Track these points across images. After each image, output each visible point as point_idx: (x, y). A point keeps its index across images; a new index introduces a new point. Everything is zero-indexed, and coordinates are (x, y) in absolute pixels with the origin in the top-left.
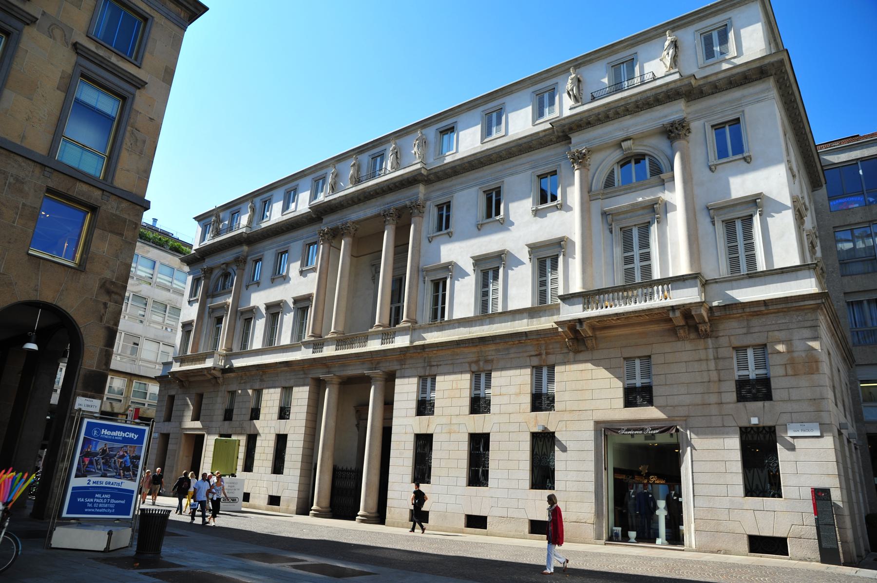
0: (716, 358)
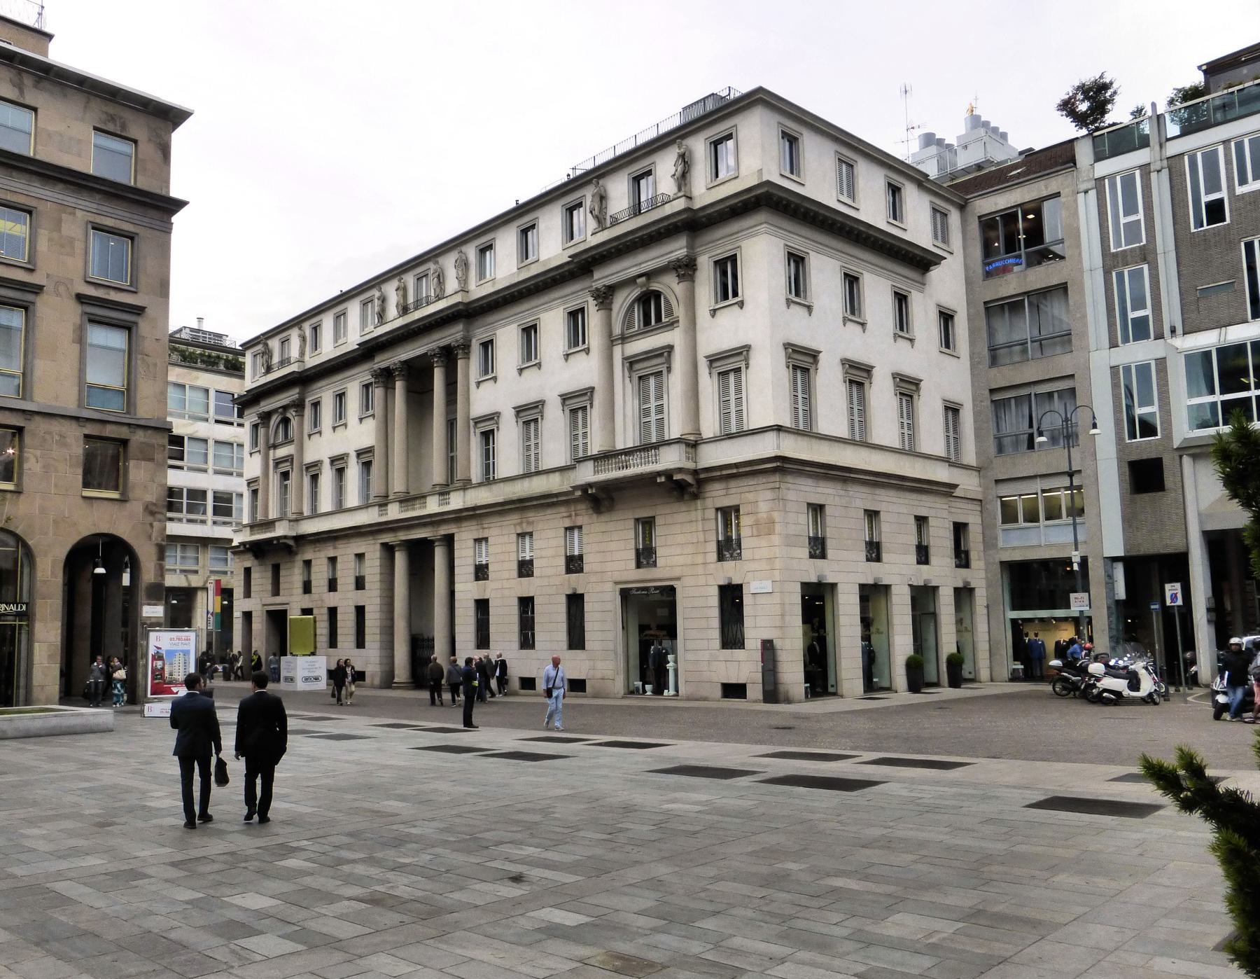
0: (703, 519)
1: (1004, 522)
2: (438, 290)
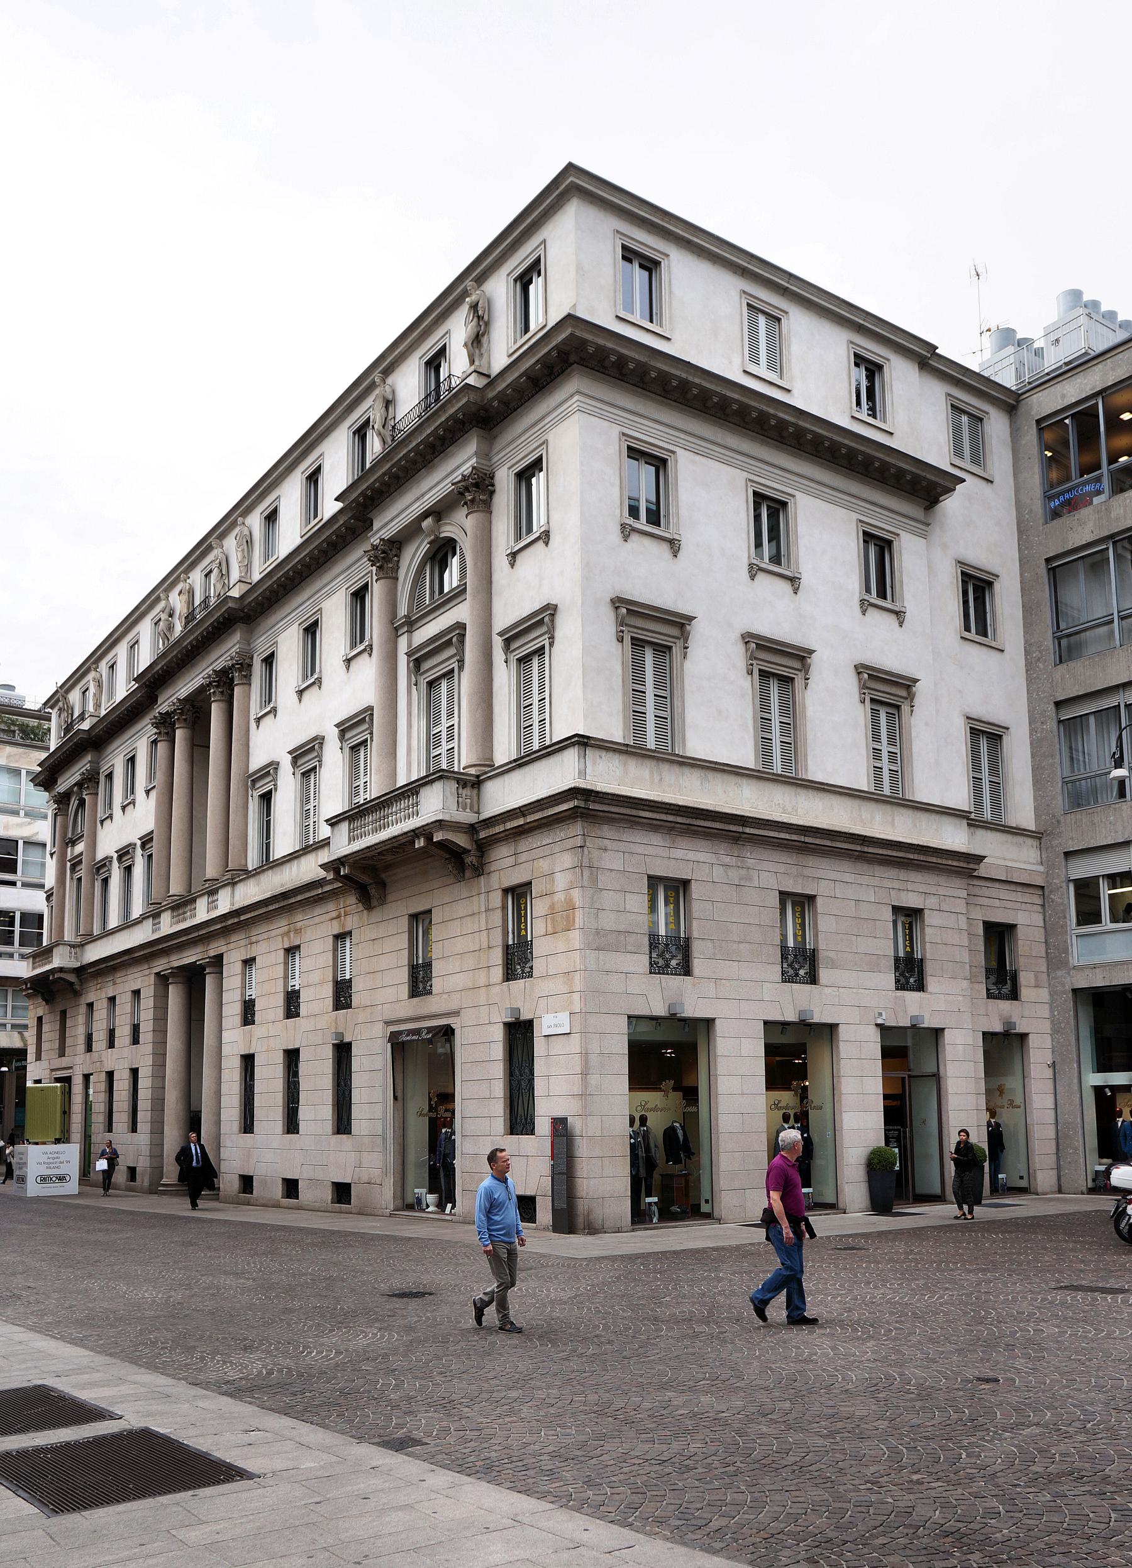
1: (1080, 923)
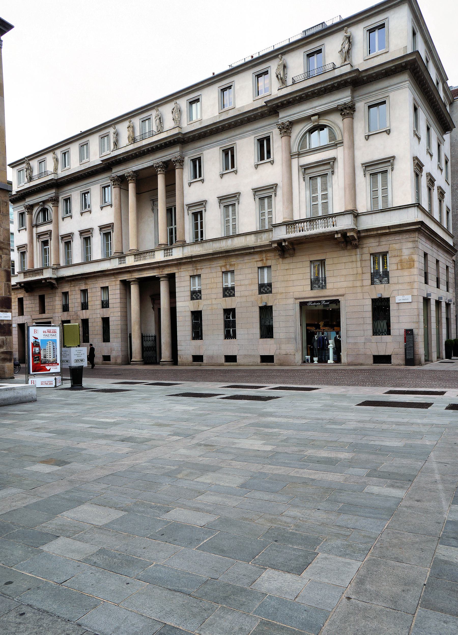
0: (361, 260)
2: (159, 127)
